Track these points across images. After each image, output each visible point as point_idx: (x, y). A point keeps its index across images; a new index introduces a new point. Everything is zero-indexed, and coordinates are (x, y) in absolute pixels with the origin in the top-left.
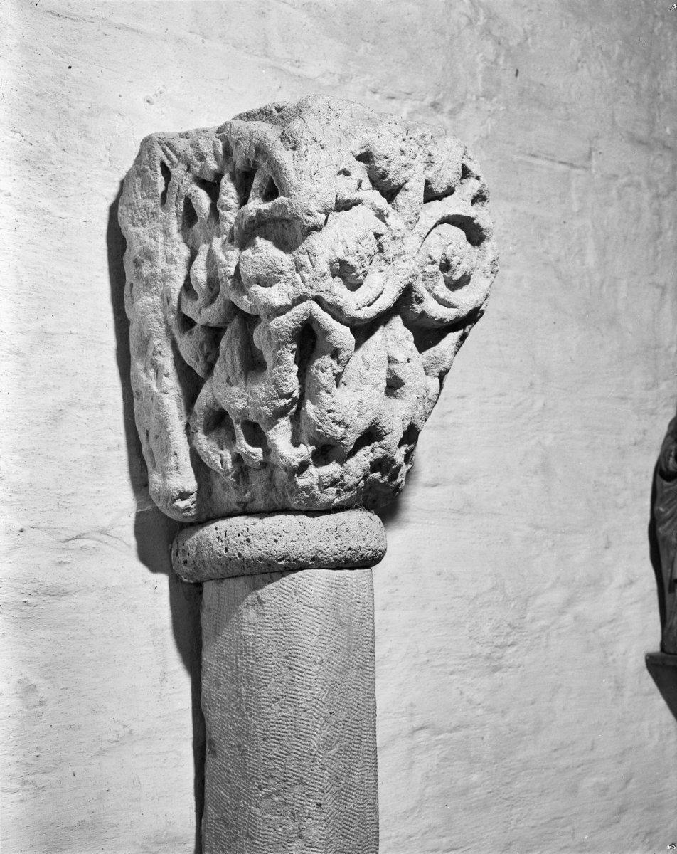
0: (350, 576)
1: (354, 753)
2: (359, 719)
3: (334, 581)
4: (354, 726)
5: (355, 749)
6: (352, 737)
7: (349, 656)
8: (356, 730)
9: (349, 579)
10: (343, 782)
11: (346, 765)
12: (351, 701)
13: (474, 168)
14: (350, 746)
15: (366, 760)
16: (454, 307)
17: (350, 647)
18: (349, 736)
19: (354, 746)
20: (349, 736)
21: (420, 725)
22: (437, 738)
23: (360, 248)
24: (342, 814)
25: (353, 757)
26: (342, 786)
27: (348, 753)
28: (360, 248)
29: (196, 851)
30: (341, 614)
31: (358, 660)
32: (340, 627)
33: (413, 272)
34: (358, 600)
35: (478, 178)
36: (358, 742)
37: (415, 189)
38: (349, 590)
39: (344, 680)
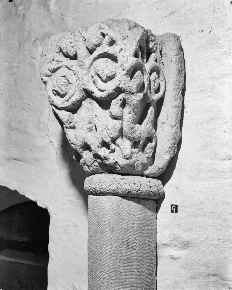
0: (99, 198)
1: (98, 264)
2: (100, 252)
3: (93, 200)
4: (99, 252)
5: (99, 262)
6: (97, 258)
7: (98, 228)
8: (99, 256)
9: (99, 199)
10: (94, 273)
11: (95, 267)
12: (98, 244)
13: (105, 32)
14: (97, 260)
15: (103, 268)
16: (105, 91)
17: (98, 224)
18: (96, 257)
19: (98, 261)
20: (96, 257)
21: (213, 273)
22: (223, 282)
23: (57, 84)
24: (93, 284)
25: (98, 265)
26: (93, 274)
27: (96, 263)
28: (57, 84)
29: (90, 286)
30: (95, 212)
31: (101, 230)
32: (95, 216)
33: (82, 84)
34: (102, 207)
35: (107, 34)
36: (100, 260)
37: (82, 53)
38: (98, 203)
39: (95, 236)
